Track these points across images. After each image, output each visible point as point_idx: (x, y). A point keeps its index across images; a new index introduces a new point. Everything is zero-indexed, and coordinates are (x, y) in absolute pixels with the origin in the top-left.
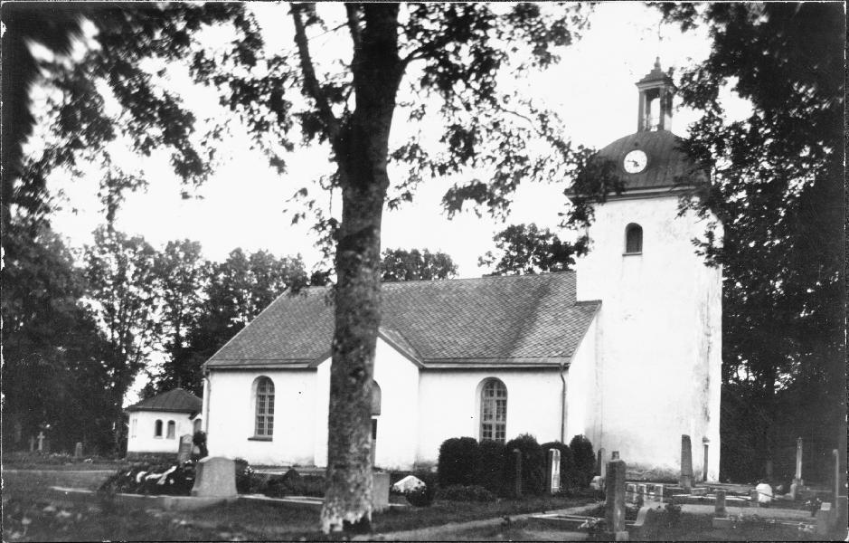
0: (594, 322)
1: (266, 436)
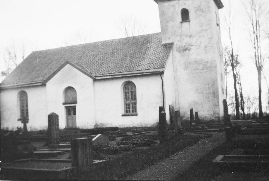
0: (171, 52)
1: (134, 113)
